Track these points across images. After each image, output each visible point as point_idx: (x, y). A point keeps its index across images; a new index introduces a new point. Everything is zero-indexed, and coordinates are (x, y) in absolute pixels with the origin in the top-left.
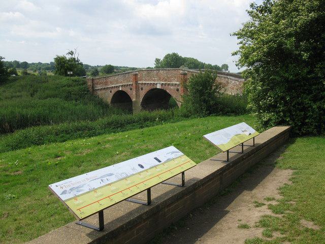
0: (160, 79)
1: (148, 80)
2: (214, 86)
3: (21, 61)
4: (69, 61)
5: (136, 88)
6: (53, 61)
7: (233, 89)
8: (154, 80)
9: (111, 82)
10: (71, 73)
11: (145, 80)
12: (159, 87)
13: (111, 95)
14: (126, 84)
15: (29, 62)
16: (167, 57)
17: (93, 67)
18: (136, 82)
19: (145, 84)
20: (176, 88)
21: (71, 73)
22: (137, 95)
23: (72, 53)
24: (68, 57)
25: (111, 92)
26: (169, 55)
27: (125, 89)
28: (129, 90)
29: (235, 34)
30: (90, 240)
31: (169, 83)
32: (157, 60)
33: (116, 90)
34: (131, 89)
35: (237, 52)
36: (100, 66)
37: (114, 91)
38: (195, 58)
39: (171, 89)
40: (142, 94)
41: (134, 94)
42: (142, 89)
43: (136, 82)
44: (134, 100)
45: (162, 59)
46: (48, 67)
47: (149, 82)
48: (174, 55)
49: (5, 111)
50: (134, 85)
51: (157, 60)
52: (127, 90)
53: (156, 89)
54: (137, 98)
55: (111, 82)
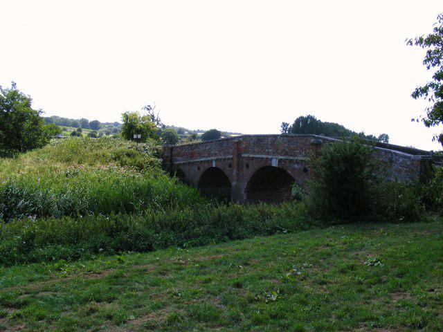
0: (277, 152)
2: (368, 167)
3: (91, 119)
4: (144, 119)
5: (238, 165)
7: (400, 172)
8: (268, 153)
9: (200, 154)
10: (139, 136)
11: (254, 153)
12: (275, 163)
13: (200, 173)
14: (224, 157)
15: (102, 120)
16: (298, 121)
17: (190, 133)
18: (239, 155)
19: (253, 158)
20: (302, 167)
21: (139, 136)
23: (149, 108)
24: (143, 113)
28: (227, 168)
29: (420, 41)
30: (441, 123)
31: (291, 158)
32: (285, 125)
33: (207, 166)
34: (230, 166)
35: (427, 88)
36: (202, 131)
37: (203, 168)
38: (340, 124)
39: (294, 169)
40: (248, 174)
42: (247, 166)
43: (239, 155)
44: (234, 184)
45: (291, 122)
46: (112, 128)
48: (310, 117)
51: (285, 125)
54: (240, 181)
55: (200, 154)
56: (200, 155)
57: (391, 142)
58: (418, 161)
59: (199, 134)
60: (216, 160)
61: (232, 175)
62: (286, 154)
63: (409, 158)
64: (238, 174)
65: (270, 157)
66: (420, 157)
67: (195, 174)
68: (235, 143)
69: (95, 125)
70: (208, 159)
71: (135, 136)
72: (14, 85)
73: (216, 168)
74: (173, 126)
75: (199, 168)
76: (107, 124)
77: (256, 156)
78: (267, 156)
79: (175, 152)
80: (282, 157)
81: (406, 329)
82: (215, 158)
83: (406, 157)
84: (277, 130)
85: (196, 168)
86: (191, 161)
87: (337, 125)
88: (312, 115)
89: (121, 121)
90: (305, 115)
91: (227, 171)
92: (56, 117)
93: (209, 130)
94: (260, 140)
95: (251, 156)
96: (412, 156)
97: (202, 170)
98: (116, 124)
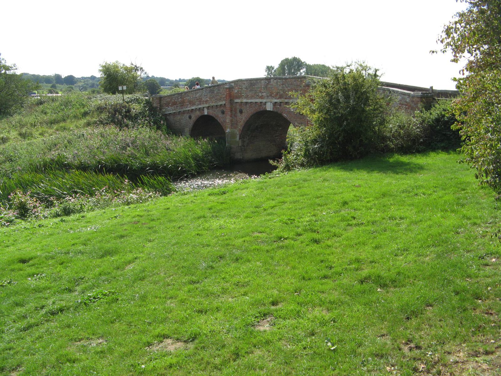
0: (271, 95)
1: (252, 97)
3: (64, 74)
5: (231, 111)
6: (174, 80)
8: (262, 97)
10: (125, 88)
11: (247, 97)
12: (269, 107)
13: (191, 122)
15: (77, 75)
18: (231, 102)
19: (246, 103)
22: (234, 124)
25: (190, 117)
26: (287, 60)
27: (212, 113)
28: (220, 115)
33: (198, 114)
34: (223, 112)
36: (184, 80)
37: (194, 117)
40: (242, 119)
41: (228, 121)
42: (241, 112)
43: (231, 102)
44: (228, 130)
45: (276, 65)
47: (254, 101)
49: (320, 202)
50: (228, 106)
51: (269, 69)
52: (217, 114)
53: (266, 112)
56: (192, 103)
57: (382, 79)
58: (418, 97)
59: (181, 83)
60: (208, 108)
61: (225, 122)
62: (281, 97)
63: (409, 95)
64: (231, 121)
65: (264, 101)
66: (420, 93)
67: (188, 123)
68: (227, 89)
69: (70, 80)
70: (200, 106)
71: (120, 88)
72: (455, 79)
73: (208, 116)
74: (153, 76)
75: (190, 117)
76: (83, 78)
77: (250, 101)
78: (261, 100)
79: (163, 102)
80: (276, 101)
81: (487, 374)
82: (207, 105)
83: (404, 94)
84: (262, 74)
85: (188, 118)
86: (182, 110)
87: (324, 66)
88: (297, 56)
89: (98, 75)
90: (290, 57)
91: (220, 118)
92: (25, 74)
93: (196, 77)
94: (252, 83)
95: (245, 101)
96: (412, 93)
97: (194, 118)
98: (93, 78)
